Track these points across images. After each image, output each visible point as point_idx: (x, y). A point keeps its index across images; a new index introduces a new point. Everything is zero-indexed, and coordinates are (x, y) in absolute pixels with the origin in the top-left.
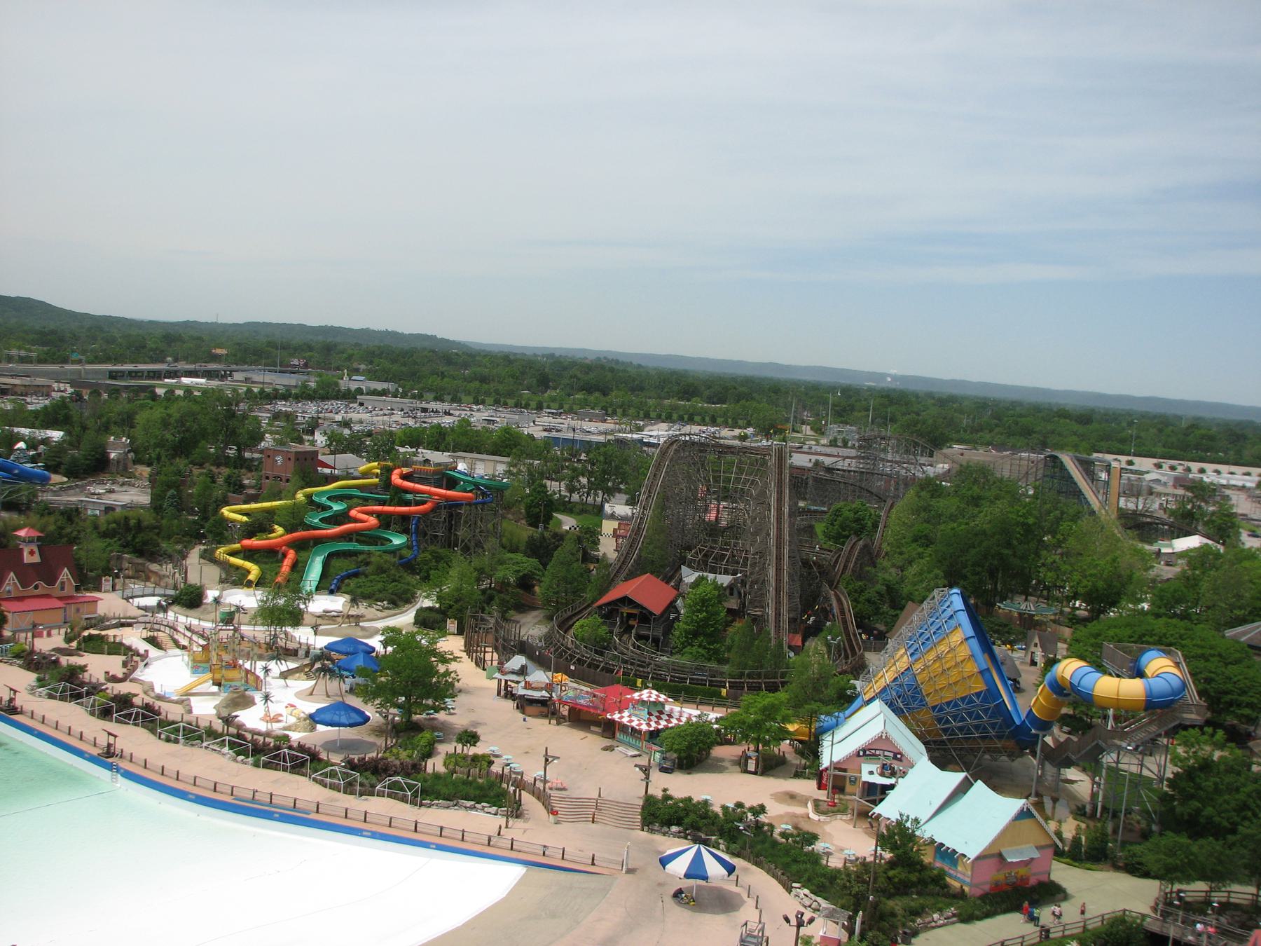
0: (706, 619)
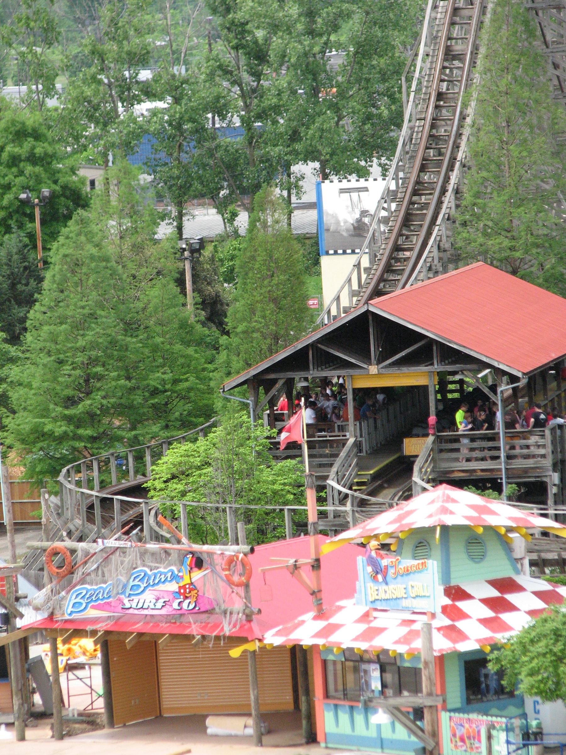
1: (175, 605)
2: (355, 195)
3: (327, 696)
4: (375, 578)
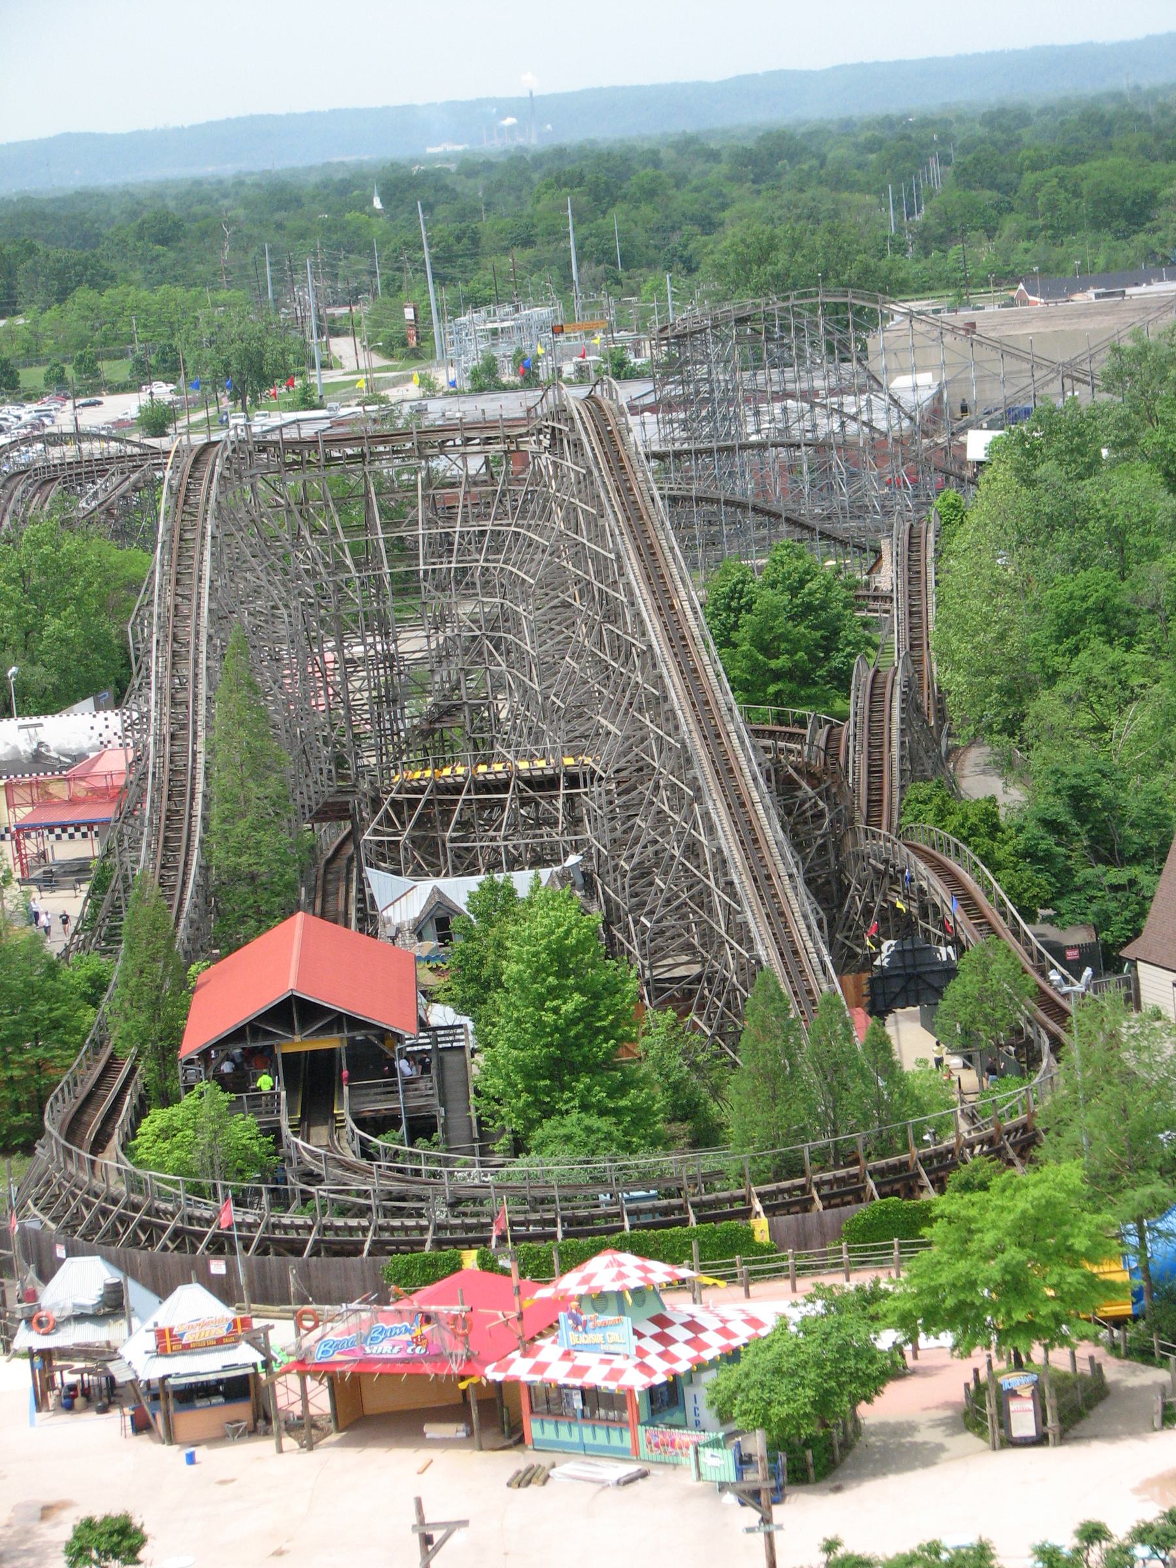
0: (586, 1014)
1: (409, 1350)
2: (32, 730)
3: (532, 1412)
4: (576, 1329)
